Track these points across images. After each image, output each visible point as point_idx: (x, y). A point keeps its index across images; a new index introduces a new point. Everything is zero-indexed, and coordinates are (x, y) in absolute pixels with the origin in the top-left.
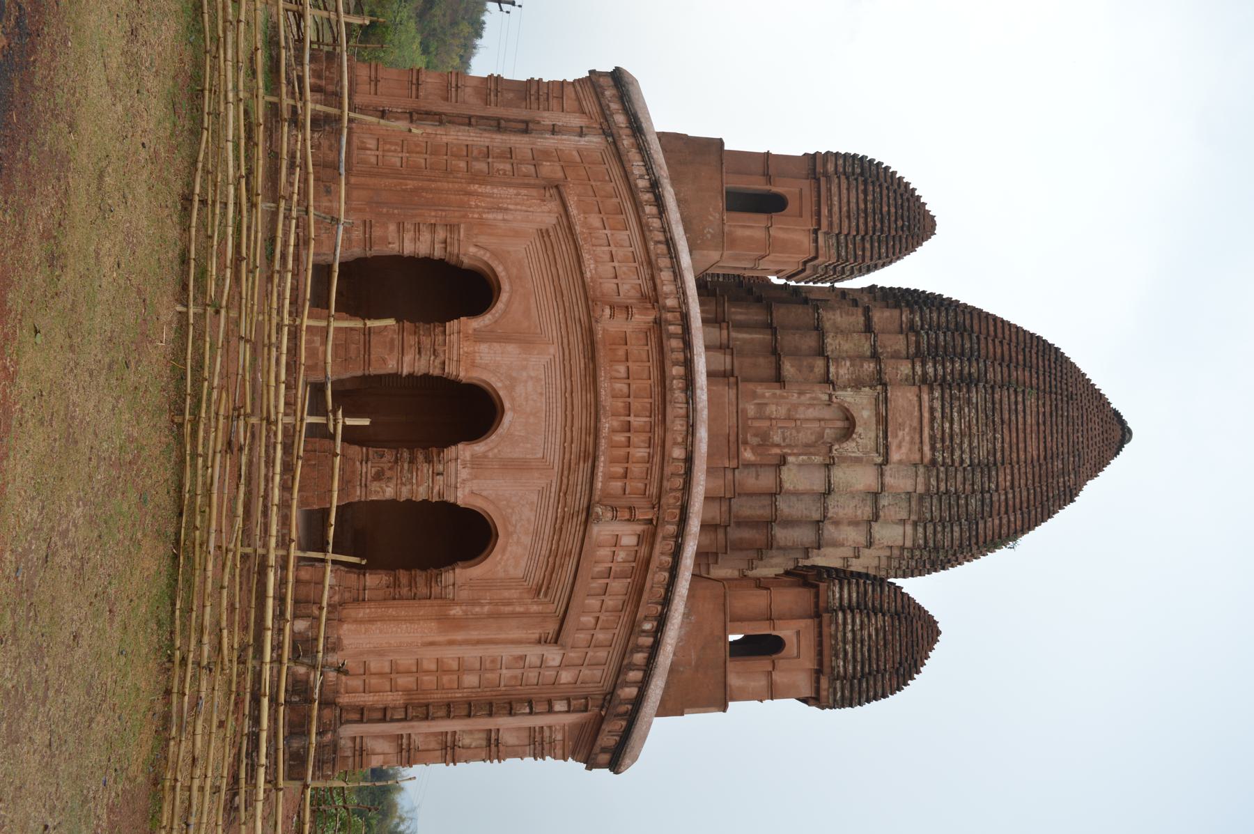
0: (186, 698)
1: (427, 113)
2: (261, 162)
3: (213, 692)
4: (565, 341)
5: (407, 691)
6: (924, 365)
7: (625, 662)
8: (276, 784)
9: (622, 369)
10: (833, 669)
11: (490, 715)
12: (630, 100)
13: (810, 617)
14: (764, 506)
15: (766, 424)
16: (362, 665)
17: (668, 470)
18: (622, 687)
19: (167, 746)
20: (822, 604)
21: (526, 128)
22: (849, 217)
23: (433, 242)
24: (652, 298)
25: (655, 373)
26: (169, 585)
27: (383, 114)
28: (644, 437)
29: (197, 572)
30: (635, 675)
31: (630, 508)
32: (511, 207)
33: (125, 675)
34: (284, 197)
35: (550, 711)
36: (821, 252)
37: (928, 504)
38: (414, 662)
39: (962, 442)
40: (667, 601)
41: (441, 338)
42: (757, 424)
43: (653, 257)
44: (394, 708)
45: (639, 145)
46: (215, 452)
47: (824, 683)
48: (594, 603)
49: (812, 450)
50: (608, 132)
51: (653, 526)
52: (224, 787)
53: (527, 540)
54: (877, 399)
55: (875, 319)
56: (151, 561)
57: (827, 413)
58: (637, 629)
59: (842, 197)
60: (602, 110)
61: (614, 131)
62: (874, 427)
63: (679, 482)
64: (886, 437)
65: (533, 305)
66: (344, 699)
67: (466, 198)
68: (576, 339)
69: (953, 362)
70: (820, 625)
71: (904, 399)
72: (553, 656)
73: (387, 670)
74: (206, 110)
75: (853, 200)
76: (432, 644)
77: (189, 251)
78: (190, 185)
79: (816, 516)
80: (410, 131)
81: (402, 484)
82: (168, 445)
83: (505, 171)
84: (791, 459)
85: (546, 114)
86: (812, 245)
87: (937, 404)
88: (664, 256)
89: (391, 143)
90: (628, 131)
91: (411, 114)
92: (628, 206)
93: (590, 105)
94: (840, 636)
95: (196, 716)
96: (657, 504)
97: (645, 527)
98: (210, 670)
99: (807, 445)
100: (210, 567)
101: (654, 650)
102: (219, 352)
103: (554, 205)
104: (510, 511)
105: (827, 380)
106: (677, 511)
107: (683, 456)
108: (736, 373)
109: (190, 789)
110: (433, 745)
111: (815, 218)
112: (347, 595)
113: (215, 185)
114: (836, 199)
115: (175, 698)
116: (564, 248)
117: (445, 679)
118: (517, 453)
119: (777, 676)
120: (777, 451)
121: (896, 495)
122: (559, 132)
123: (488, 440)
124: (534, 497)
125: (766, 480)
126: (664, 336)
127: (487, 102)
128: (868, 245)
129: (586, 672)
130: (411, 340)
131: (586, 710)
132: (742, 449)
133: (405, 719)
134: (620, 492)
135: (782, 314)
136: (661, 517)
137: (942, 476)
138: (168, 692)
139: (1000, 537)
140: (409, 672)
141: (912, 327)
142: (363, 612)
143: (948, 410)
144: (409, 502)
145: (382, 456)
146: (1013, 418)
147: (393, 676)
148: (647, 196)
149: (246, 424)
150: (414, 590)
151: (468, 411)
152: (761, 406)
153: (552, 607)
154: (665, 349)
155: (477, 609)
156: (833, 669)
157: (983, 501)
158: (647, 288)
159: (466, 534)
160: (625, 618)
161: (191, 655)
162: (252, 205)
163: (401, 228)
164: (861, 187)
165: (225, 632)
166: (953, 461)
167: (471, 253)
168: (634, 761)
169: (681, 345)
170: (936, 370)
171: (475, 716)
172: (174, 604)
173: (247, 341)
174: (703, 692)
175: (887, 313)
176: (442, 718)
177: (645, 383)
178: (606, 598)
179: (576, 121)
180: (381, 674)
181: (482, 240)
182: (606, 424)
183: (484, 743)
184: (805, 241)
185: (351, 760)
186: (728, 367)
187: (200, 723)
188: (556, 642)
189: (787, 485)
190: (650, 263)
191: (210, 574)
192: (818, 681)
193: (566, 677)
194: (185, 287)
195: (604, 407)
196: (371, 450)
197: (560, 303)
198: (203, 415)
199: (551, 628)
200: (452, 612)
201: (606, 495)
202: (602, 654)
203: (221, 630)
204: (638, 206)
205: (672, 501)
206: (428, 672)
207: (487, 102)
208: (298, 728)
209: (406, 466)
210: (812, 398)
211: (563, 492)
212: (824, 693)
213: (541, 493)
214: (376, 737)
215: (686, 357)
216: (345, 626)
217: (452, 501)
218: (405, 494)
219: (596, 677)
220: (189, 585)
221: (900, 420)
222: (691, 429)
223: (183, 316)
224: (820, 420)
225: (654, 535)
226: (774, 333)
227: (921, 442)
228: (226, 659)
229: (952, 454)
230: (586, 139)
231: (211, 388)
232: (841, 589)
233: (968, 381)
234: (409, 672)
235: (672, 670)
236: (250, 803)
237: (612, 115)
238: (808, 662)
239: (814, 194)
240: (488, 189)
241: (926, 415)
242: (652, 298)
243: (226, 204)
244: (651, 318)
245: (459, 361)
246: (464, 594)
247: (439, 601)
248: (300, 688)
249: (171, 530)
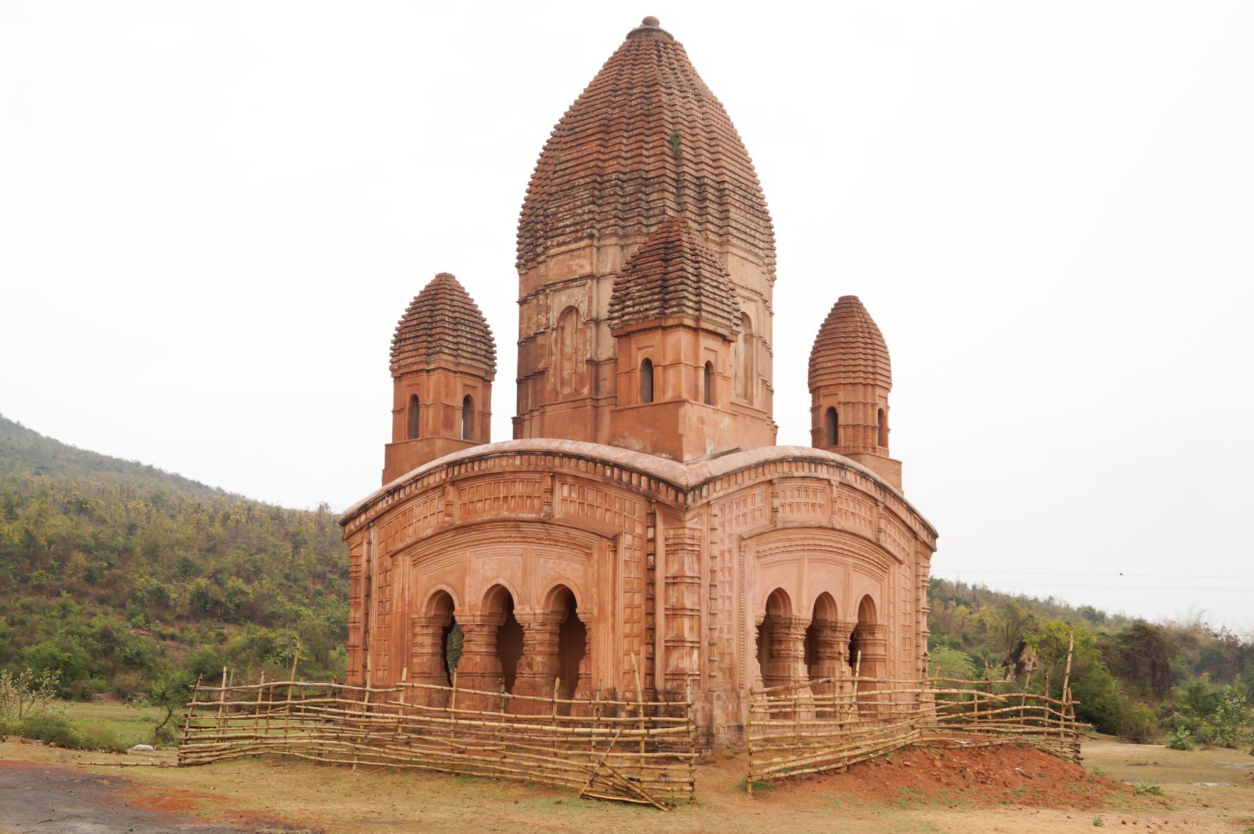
9: (479, 505)
21: (369, 578)
47: (670, 322)
54: (555, 291)
64: (576, 280)
72: (626, 540)
76: (613, 628)
87: (556, 240)
92: (402, 508)
116: (421, 549)
117: (636, 617)
118: (519, 573)
119: (668, 361)
124: (542, 560)
167: (423, 609)
181: (419, 603)
184: (434, 377)
192: (671, 327)
199: (606, 543)
206: (632, 629)
213: (539, 556)
225: (561, 474)
238: (656, 337)
241: (563, 248)
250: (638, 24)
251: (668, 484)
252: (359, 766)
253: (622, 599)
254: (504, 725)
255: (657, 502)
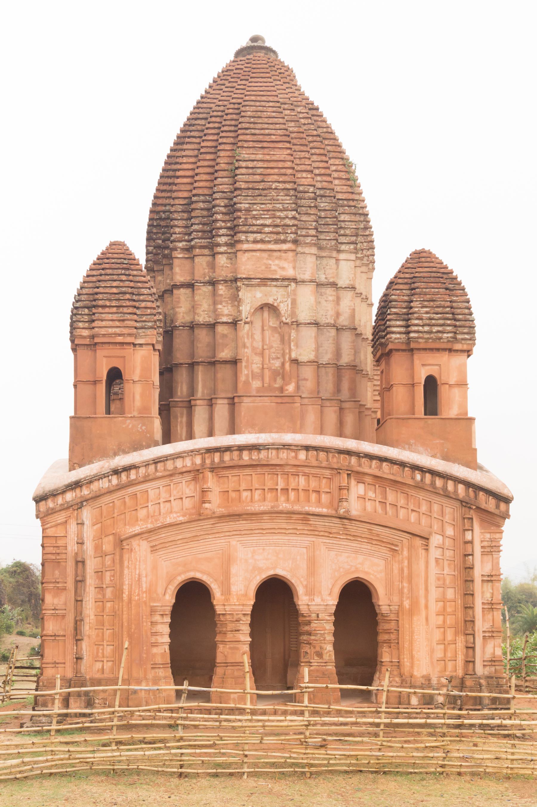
0: (463, 764)
1: (76, 629)
2: (155, 735)
3: (459, 750)
4: (228, 534)
5: (456, 634)
6: (219, 245)
7: (442, 492)
8: (512, 714)
9: (245, 494)
10: (449, 341)
11: (472, 581)
12: (56, 490)
13: (412, 355)
14: (327, 373)
15: (267, 372)
16: (439, 662)
17: (314, 463)
18: (458, 495)
19: (488, 773)
20: (404, 347)
21: (80, 563)
22: (123, 320)
23: (162, 623)
24: (196, 474)
25: (248, 471)
26: (401, 775)
27: (79, 659)
28: (291, 479)
29: (394, 761)
30: (450, 485)
31: (340, 489)
32: (137, 572)
33: (454, 794)
34: (175, 721)
35: (471, 542)
36: (150, 342)
37: (325, 243)
38: (438, 630)
39: (280, 218)
40: (402, 464)
41: (228, 617)
42: (267, 379)
43: (168, 473)
44: (466, 642)
45: (87, 483)
46: (327, 754)
47: (458, 346)
48: (402, 513)
49: (286, 338)
50: (80, 505)
51: (351, 473)
52: (512, 742)
53: (361, 558)
54: (248, 286)
55: (182, 279)
56: (389, 784)
57: (258, 324)
58: (420, 485)
59: (108, 325)
60: (64, 509)
61: (79, 501)
62: (268, 289)
63: (322, 455)
64: (276, 280)
65: (203, 555)
66: (460, 673)
67: (133, 603)
68: (225, 526)
69: (216, 221)
70: (419, 349)
71: (247, 264)
72: (436, 540)
73: (442, 646)
74: (126, 767)
75: (110, 316)
76: (427, 619)
77: (210, 773)
78: (172, 774)
79: (333, 332)
80: (126, 648)
81: (324, 640)
82: (324, 779)
83: (111, 576)
84: (293, 356)
85: (69, 548)
86: (144, 347)
87: (251, 237)
88: (165, 465)
89: (97, 653)
90: (78, 490)
91: (77, 640)
92: (131, 490)
93: (60, 517)
94: (426, 336)
95: (473, 758)
96: (338, 471)
97: (352, 478)
98: (448, 752)
99: (282, 340)
100: (391, 754)
101: (434, 473)
102: (269, 754)
103: (135, 543)
104: (341, 570)
105: (234, 324)
106: (342, 456)
107: (304, 452)
108: (230, 396)
109: (513, 760)
110: (490, 617)
111: (125, 346)
112: (395, 673)
113: (171, 760)
114: (110, 330)
115: (463, 770)
116: (164, 535)
117: (449, 610)
118: (303, 565)
120: (287, 366)
121: (318, 269)
122: (82, 539)
123: (295, 584)
124: (333, 553)
125: (308, 372)
126: (223, 465)
127: (65, 589)
128: (143, 304)
129: (447, 518)
130: (230, 636)
131: (472, 519)
132: (286, 393)
133: (474, 635)
134: (328, 495)
135: (181, 355)
136: (345, 467)
137: (304, 232)
138: (459, 774)
139: (348, 179)
140: (444, 633)
141: (189, 249)
142: (406, 663)
143: (255, 229)
144: (335, 635)
145: (307, 653)
146: (259, 171)
147: (446, 643)
148: (124, 476)
149: (310, 738)
150: (392, 631)
151: (275, 594)
152: (254, 376)
153: (405, 541)
154: (231, 465)
155: (406, 590)
156: (449, 341)
157: (322, 196)
158: (189, 477)
159: (356, 597)
160: (412, 492)
161: (440, 762)
162: (181, 739)
163: (155, 645)
164: (100, 310)
165: (427, 745)
166: (293, 225)
168: (504, 486)
169: (228, 453)
170: (223, 235)
171: (473, 591)
172: (411, 773)
173: (262, 739)
174: (460, 437)
175: (177, 270)
176: (473, 612)
177: (255, 478)
178: (399, 505)
179: (73, 527)
180: (445, 650)
182: (284, 506)
183: (490, 584)
185: (497, 667)
186: (226, 401)
187: (476, 756)
188: (428, 539)
189: (312, 357)
190: (171, 475)
191: (395, 754)
193: (450, 531)
194: (231, 774)
195: (272, 507)
196: (303, 660)
197: (201, 537)
198: (306, 761)
199: (418, 542)
200: (407, 606)
201: (331, 505)
202: (436, 508)
203: (426, 747)
204: (131, 484)
205: (335, 460)
207: (65, 589)
208: (478, 702)
209: (313, 638)
210: (248, 338)
211: (329, 534)
212: (465, 347)
213: (330, 549)
214: (484, 652)
215: (237, 450)
216: (415, 673)
217: (335, 607)
218: (330, 638)
219: (451, 511)
220: (398, 765)
221: (263, 268)
222: (286, 447)
223: (250, 774)
224: (263, 330)
225: (358, 473)
226: (198, 363)
227: (280, 251)
228: (443, 743)
229: (288, 226)
230: (85, 520)
231: (290, 758)
232: (393, 333)
233: (232, 209)
234: (444, 633)
235: (446, 458)
236: (521, 728)
237: (67, 503)
238: (444, 358)
239: (106, 346)
240: (126, 588)
241: (259, 246)
242: (196, 474)
243: (182, 754)
244: (210, 475)
245: (243, 605)
246: (396, 599)
247: (400, 614)
248: (452, 701)
249: (371, 776)
250: (244, 42)
251: (489, 492)
252: (250, 774)
253: (434, 593)
254: (466, 722)
255: (478, 508)
